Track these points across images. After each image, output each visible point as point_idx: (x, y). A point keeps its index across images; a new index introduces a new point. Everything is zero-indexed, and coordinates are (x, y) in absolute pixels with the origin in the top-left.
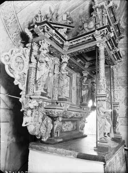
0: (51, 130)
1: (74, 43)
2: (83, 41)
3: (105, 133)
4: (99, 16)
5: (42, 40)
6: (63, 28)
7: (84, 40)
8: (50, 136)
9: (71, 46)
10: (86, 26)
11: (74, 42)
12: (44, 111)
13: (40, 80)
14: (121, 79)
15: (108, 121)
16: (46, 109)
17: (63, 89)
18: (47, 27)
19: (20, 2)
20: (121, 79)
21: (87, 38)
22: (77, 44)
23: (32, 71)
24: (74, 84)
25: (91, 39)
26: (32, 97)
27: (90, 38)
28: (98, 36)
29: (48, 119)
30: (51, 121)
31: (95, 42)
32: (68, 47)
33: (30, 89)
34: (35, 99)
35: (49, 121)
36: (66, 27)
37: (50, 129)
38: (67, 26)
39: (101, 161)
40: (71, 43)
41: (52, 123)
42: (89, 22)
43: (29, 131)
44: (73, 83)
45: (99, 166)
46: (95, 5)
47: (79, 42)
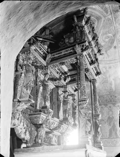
0: (35, 137)
1: (56, 56)
2: (65, 53)
3: (86, 132)
4: (79, 33)
5: (27, 51)
6: (46, 42)
7: (66, 52)
8: (34, 142)
9: (53, 58)
10: (67, 41)
11: (57, 54)
12: (28, 118)
13: (27, 85)
14: (107, 101)
15: (89, 121)
16: (31, 116)
17: (46, 98)
18: (33, 40)
19: (118, 51)
20: (107, 101)
21: (69, 51)
22: (58, 56)
23: (18, 79)
24: (54, 99)
25: (72, 52)
26: (20, 100)
27: (72, 51)
28: (93, 94)
29: (32, 126)
30: (35, 128)
31: (76, 55)
32: (51, 60)
33: (18, 95)
34: (23, 101)
35: (33, 129)
36: (48, 41)
37: (34, 136)
38: (50, 40)
39: (83, 148)
40: (54, 55)
41: (36, 131)
42: (70, 37)
43: (16, 133)
44: (53, 98)
45: (82, 153)
46: (75, 23)
47: (61, 54)
